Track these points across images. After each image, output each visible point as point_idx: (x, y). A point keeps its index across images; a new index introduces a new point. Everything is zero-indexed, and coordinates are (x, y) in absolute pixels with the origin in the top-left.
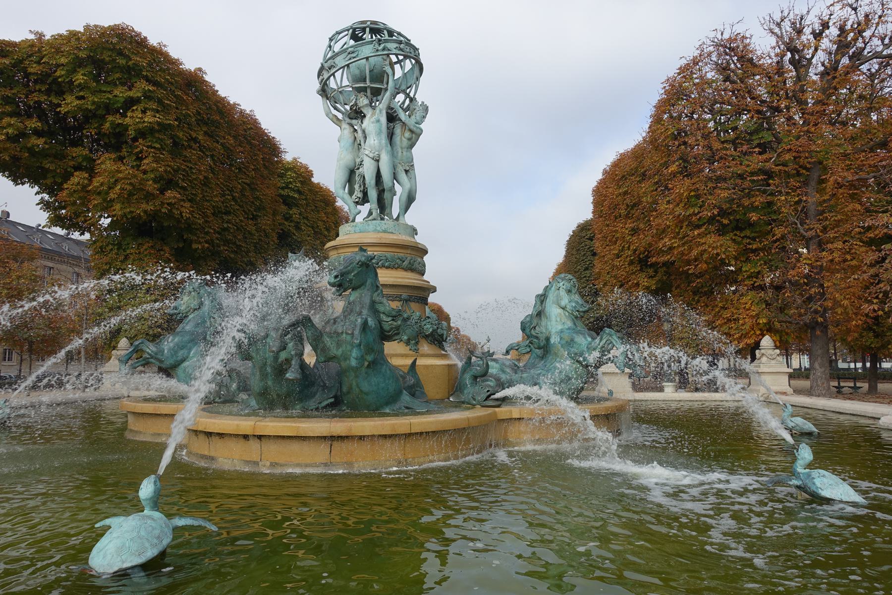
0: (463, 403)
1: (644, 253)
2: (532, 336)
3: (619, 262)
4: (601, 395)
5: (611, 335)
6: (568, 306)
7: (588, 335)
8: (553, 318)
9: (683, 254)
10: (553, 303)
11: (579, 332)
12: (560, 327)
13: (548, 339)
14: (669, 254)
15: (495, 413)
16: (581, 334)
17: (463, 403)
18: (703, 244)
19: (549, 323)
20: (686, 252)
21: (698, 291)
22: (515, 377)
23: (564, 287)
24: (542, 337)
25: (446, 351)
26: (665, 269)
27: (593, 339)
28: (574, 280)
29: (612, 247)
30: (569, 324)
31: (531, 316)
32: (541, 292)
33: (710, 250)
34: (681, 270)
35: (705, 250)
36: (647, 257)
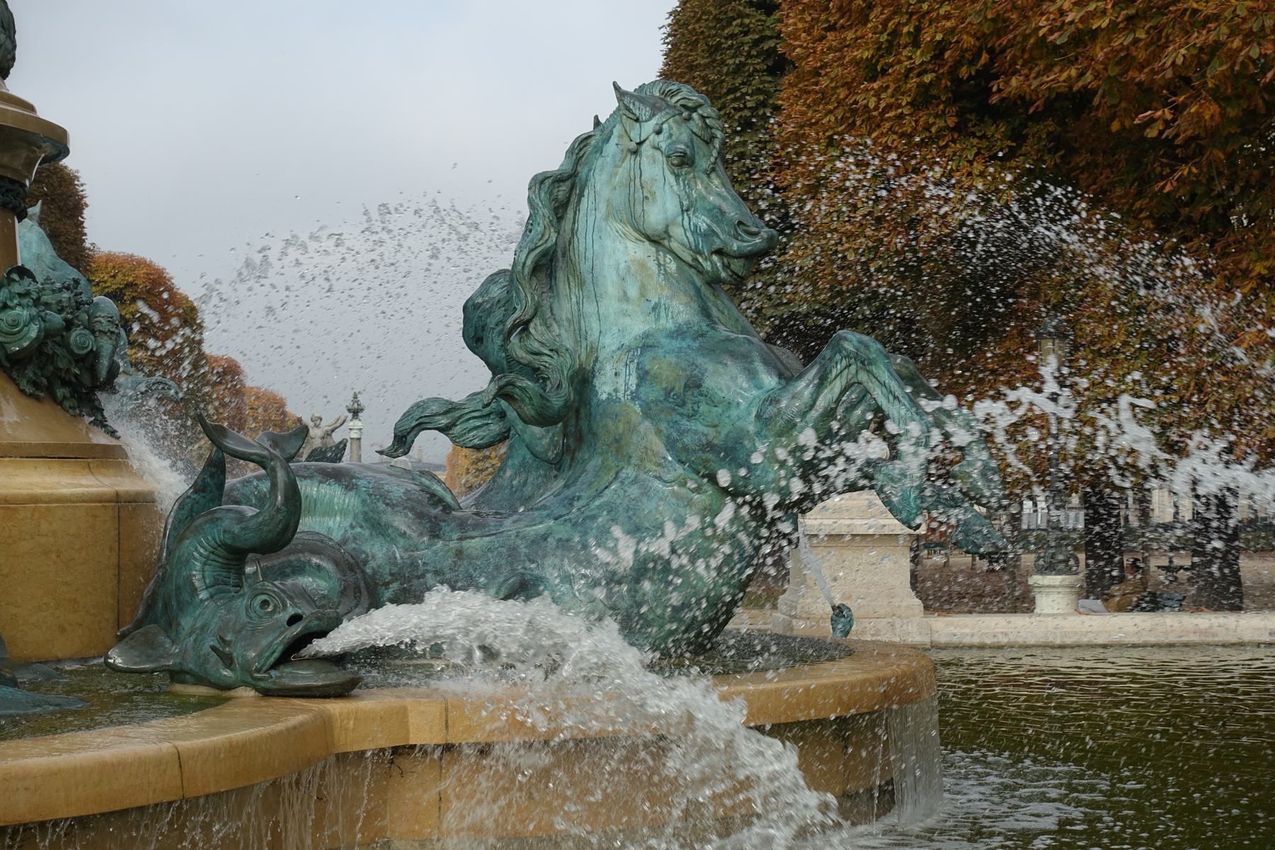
0: (176, 675)
1: (972, 62)
2: (513, 364)
3: (877, 94)
4: (801, 627)
5: (865, 363)
6: (677, 232)
7: (766, 362)
8: (610, 285)
9: (1125, 60)
10: (611, 213)
11: (723, 350)
12: (637, 326)
13: (583, 380)
14: (1072, 62)
15: (326, 724)
16: (733, 354)
17: (176, 675)
18: (1208, 19)
19: (589, 308)
20: (1141, 55)
21: (1175, 216)
22: (432, 552)
23: (662, 140)
24: (558, 368)
25: (113, 433)
26: (1050, 125)
27: (786, 377)
28: (707, 111)
29: (850, 35)
30: (681, 311)
31: (510, 278)
32: (555, 161)
33: (1236, 43)
34: (1115, 126)
35: (1218, 45)
36: (987, 75)
